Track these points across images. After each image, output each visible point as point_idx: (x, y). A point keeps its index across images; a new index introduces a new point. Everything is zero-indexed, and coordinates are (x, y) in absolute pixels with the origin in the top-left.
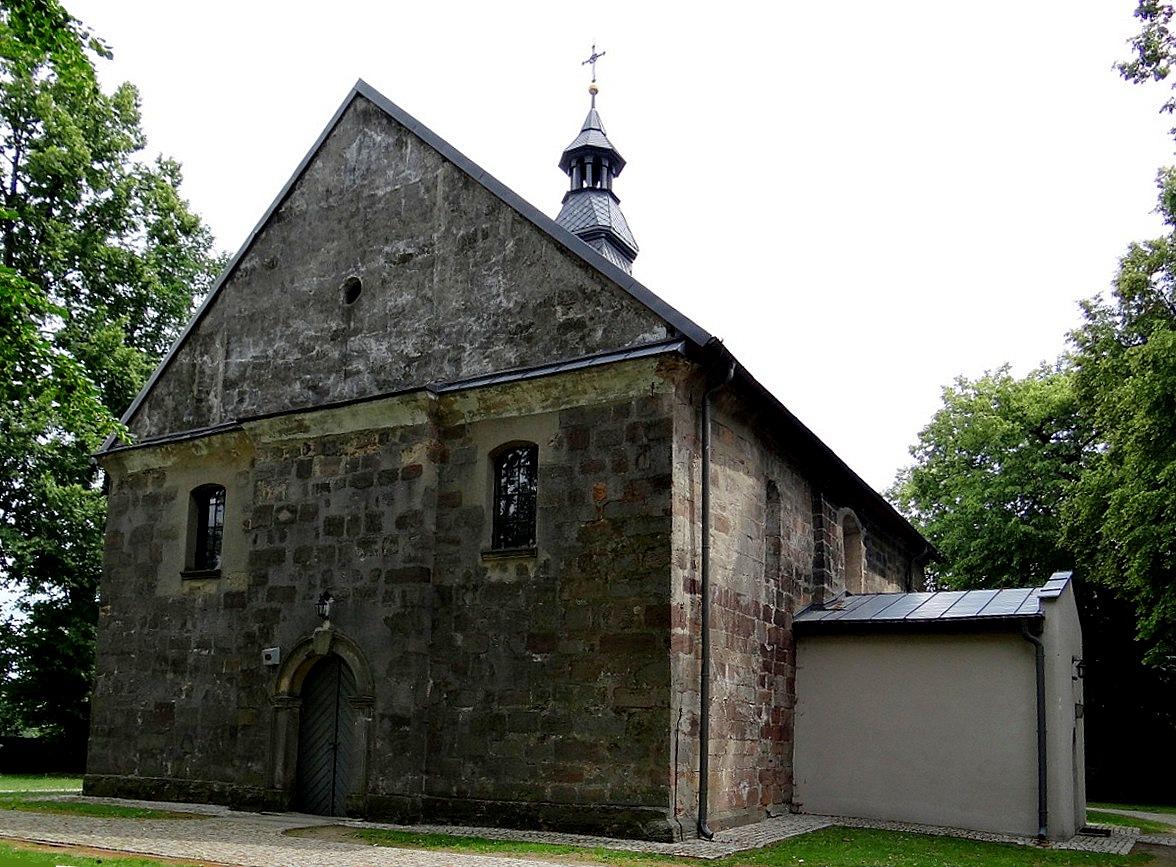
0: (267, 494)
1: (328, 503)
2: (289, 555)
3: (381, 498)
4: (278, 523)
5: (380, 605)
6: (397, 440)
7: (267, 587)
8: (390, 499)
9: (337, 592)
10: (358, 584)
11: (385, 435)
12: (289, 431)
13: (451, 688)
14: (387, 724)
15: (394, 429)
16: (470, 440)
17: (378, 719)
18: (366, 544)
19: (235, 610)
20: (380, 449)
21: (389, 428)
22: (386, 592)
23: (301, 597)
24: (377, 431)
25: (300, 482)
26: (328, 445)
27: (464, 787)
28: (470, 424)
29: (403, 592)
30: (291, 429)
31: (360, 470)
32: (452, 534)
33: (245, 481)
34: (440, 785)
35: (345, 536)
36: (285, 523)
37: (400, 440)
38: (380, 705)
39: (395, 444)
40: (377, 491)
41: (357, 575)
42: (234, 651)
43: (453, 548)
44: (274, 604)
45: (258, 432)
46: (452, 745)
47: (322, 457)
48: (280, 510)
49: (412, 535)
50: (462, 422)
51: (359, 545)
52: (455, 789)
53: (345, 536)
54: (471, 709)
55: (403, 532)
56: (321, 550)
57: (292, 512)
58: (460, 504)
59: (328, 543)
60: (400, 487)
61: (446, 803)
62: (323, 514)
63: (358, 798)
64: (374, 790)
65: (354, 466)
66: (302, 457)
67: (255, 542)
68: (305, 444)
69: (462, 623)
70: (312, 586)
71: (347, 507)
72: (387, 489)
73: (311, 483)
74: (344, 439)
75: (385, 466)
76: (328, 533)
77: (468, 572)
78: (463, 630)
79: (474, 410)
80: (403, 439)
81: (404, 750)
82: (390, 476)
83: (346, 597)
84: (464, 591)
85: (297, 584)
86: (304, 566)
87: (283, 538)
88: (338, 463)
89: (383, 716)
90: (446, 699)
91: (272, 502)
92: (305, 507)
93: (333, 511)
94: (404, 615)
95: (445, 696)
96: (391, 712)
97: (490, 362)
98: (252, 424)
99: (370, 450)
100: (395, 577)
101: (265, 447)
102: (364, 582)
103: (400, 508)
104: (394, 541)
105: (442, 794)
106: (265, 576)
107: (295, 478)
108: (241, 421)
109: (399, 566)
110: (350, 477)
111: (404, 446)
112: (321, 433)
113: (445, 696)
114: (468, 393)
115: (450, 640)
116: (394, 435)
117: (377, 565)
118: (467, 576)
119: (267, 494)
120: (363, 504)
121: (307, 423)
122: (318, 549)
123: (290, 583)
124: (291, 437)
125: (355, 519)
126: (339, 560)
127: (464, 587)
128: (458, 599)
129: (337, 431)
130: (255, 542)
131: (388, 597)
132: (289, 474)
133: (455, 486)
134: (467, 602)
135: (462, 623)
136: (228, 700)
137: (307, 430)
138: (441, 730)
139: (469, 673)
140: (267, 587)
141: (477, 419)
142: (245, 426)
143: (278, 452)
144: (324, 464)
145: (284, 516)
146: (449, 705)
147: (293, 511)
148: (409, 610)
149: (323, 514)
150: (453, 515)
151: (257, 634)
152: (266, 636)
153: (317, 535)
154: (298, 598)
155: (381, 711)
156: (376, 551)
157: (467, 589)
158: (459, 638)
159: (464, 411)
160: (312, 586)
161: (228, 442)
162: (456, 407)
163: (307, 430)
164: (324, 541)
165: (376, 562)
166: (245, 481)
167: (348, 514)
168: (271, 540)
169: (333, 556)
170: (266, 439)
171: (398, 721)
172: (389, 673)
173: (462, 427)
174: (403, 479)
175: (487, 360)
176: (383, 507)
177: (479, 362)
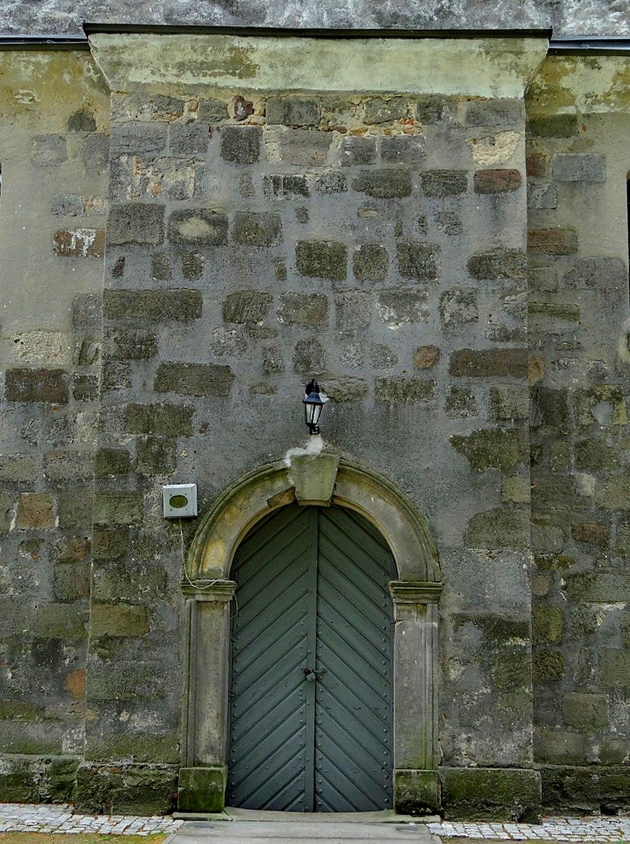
0: (146, 181)
1: (303, 215)
2: (212, 306)
3: (430, 220)
4: (178, 242)
5: (440, 412)
6: (461, 119)
7: (155, 364)
8: (454, 225)
9: (335, 384)
10: (388, 373)
11: (431, 108)
12: (201, 68)
13: (573, 569)
14: (472, 634)
15: (452, 101)
16: (590, 143)
17: (450, 626)
18: (401, 301)
19: (37, 404)
20: (423, 131)
21: (442, 97)
22: (454, 391)
23: (246, 388)
24: (413, 98)
25: (232, 169)
26: (296, 108)
27: (616, 746)
28: (587, 116)
29: (494, 392)
30: (212, 66)
31: (378, 165)
32: (559, 301)
33: (54, 155)
34: (564, 743)
35: (350, 279)
36: (198, 243)
37: (468, 119)
38: (454, 601)
39: (458, 126)
40: (416, 205)
41: (384, 355)
42: (40, 487)
43: (560, 325)
44: (174, 398)
45: (126, 57)
46: (585, 671)
47: (285, 129)
48: (182, 216)
49: (511, 292)
50: (570, 110)
51: (383, 299)
52: (596, 749)
53: (350, 279)
54: (621, 606)
55: (486, 286)
56: (293, 303)
57: (213, 223)
58: (575, 250)
59: (309, 291)
60: (472, 207)
61: (587, 775)
62: (293, 234)
63: (426, 777)
64: (447, 759)
65: (362, 154)
66: (232, 122)
67: (118, 270)
68: (241, 99)
69: (590, 456)
70: (270, 369)
71: (354, 228)
72: (447, 204)
73: (259, 174)
74: (339, 103)
75: (436, 161)
76: (309, 272)
77: (597, 369)
78: (594, 470)
79: (600, 93)
80: (475, 118)
81: (515, 682)
82: (451, 184)
83: (358, 395)
84: (592, 400)
85: (233, 362)
86: (251, 329)
87: (192, 270)
88: (325, 144)
89: (461, 620)
90: (565, 588)
91: (162, 200)
92: (243, 219)
93: (319, 230)
94: (498, 433)
95: (563, 583)
96: (482, 612)
97: (622, 18)
98: (118, 40)
99: (398, 130)
100: (465, 364)
101: (139, 93)
102: (404, 368)
103: (476, 242)
104: (468, 299)
105: (567, 758)
106: (151, 341)
107: (219, 161)
108: (90, 29)
109: (482, 344)
110: (354, 173)
111: (477, 132)
112: (280, 84)
113: (563, 583)
114: (602, 60)
115: (569, 490)
116: (454, 109)
117: (429, 341)
118: (598, 376)
119: (146, 181)
120: (390, 226)
121: (255, 58)
122: (283, 299)
123: (215, 360)
124: (205, 80)
125: (372, 254)
126: (339, 325)
127: (590, 393)
128: (579, 413)
129: (321, 85)
130: (118, 270)
131: (458, 400)
132: (204, 148)
133: (561, 218)
134: (600, 420)
135: (590, 456)
136: (23, 586)
137: (248, 71)
138: (560, 644)
139: (612, 542)
140: (155, 364)
141: (601, 109)
142: (97, 40)
143: (168, 104)
144: (286, 142)
145: (193, 229)
146: (573, 599)
147: (218, 222)
148: (511, 425)
149: (293, 234)
150: (561, 268)
151: (133, 454)
152: (160, 460)
153: (282, 274)
154: (236, 392)
155: (456, 610)
156: (426, 314)
157: (599, 398)
158: (588, 483)
159: (579, 92)
160: (270, 369)
161: (17, 71)
162: (565, 82)
163: (248, 71)
164: (295, 284)
165: (429, 333)
166: (54, 155)
167: (357, 242)
168: (159, 271)
169: (322, 316)
170: (136, 76)
171: (497, 629)
172: (470, 539)
173: (572, 120)
174: (479, 190)
175: (618, 14)
176: (436, 235)
177: (602, 15)
